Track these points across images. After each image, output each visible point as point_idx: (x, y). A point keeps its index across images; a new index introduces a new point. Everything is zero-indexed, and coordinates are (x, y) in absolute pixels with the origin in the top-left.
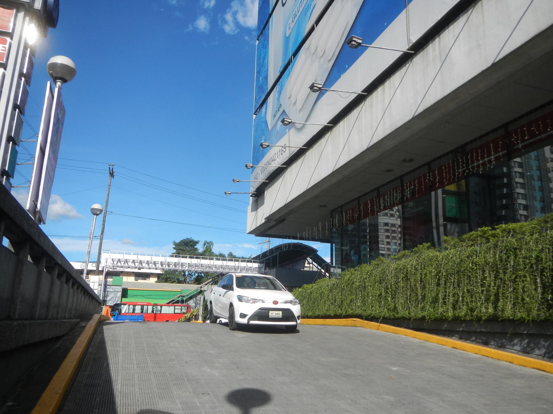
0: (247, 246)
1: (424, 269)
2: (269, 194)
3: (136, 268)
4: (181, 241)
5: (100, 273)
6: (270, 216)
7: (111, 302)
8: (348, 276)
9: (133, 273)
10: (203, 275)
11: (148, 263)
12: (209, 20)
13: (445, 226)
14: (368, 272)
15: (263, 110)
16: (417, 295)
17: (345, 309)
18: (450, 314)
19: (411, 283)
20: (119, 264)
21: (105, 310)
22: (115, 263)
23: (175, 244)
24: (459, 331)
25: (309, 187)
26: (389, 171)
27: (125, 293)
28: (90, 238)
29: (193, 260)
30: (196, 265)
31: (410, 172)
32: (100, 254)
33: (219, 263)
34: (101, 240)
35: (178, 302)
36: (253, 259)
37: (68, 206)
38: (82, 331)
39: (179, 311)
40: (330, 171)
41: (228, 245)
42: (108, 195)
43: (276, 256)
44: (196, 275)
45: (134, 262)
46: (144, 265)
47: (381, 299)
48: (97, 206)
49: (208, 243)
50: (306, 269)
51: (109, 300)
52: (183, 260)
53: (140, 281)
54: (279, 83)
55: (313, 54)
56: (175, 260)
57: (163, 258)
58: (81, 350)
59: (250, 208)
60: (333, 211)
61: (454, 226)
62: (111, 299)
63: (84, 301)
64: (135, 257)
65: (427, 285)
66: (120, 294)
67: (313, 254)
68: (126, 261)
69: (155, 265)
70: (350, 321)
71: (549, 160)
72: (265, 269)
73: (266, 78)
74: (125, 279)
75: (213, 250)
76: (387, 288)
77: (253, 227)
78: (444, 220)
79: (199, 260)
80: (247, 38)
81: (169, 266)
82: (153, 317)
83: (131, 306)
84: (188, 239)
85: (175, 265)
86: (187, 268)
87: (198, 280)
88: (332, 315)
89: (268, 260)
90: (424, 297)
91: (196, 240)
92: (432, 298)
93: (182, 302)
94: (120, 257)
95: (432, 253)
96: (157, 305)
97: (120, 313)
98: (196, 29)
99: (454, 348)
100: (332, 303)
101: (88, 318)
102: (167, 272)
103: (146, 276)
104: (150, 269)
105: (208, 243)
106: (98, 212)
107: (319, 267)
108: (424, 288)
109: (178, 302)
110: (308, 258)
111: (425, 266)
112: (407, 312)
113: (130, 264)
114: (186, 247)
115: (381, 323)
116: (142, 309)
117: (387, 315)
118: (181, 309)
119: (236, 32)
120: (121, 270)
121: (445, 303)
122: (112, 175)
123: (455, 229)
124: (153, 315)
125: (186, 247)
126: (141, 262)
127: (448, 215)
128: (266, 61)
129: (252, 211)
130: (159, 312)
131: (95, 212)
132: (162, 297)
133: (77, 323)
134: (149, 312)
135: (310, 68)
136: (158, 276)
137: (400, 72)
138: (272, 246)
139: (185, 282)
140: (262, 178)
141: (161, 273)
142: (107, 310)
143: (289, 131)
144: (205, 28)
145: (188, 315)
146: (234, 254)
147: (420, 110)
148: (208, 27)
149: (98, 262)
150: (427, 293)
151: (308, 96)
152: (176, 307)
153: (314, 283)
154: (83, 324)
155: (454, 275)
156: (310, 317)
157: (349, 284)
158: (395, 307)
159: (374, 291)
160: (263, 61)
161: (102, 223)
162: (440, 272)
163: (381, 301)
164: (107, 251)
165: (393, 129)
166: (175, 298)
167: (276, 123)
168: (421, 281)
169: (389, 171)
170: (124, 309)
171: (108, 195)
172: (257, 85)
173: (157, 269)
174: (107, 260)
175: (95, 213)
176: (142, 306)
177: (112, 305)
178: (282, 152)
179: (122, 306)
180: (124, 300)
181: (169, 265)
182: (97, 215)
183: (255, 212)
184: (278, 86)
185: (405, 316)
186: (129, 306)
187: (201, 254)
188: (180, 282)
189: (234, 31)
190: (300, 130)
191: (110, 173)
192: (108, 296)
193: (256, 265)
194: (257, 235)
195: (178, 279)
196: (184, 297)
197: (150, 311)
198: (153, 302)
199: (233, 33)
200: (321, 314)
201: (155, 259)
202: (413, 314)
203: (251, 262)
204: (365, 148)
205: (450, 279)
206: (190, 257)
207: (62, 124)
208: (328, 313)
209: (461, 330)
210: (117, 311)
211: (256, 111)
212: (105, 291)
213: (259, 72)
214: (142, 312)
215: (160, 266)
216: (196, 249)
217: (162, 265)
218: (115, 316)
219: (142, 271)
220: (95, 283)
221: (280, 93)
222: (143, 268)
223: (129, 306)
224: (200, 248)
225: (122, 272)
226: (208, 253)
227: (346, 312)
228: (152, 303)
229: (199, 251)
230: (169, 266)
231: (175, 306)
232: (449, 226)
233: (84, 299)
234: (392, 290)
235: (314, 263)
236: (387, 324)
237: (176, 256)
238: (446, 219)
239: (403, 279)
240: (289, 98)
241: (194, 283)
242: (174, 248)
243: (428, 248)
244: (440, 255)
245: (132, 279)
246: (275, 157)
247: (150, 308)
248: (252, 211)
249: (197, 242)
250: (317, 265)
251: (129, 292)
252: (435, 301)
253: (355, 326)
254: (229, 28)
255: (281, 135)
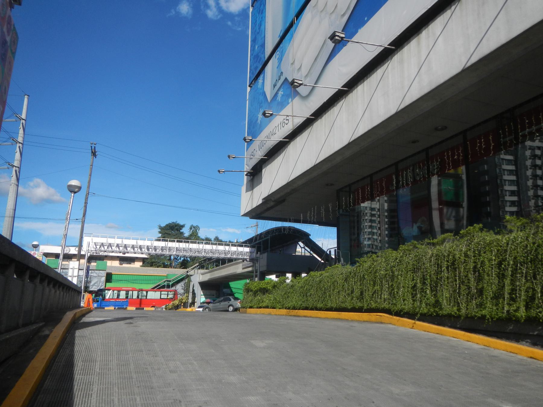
0: (230, 230)
1: (480, 255)
2: (267, 172)
3: (120, 252)
4: (167, 225)
5: (80, 257)
6: (268, 196)
7: (94, 287)
8: (369, 263)
9: (118, 257)
10: (189, 259)
11: (133, 247)
12: (191, 5)
13: (441, 211)
14: (397, 259)
15: (260, 80)
16: (469, 288)
17: (367, 301)
18: (522, 313)
19: (460, 273)
20: (102, 249)
21: (85, 300)
22: (98, 247)
23: (161, 228)
24: (534, 335)
25: (318, 162)
26: (414, 142)
27: (109, 278)
28: (67, 219)
29: (181, 244)
30: (184, 250)
31: (440, 143)
32: (81, 238)
33: (208, 247)
34: (83, 223)
35: (163, 287)
36: (243, 243)
37: (52, 190)
38: (42, 345)
39: (165, 297)
40: (345, 142)
41: (212, 230)
42: (90, 175)
43: (268, 240)
44: (182, 259)
45: (118, 246)
46: (129, 249)
47: (416, 290)
48: (74, 183)
49: (194, 228)
50: (297, 254)
51: (93, 285)
52: (170, 244)
53: (125, 265)
54: (279, 49)
55: (322, 11)
56: (162, 244)
57: (150, 242)
58: (27, 393)
59: (244, 188)
60: (339, 191)
61: (450, 210)
62: (95, 283)
63: (55, 295)
64: (119, 241)
65: (486, 277)
66: (104, 279)
67: (305, 238)
68: (110, 245)
69: (141, 250)
70: (373, 316)
71: (528, 147)
72: (257, 253)
73: (263, 46)
74: (109, 263)
75: (199, 235)
76: (424, 279)
77: (249, 209)
78: (440, 204)
79: (187, 244)
80: (229, 23)
81: (155, 250)
82: (139, 303)
83: (115, 292)
84: (173, 223)
85: (162, 249)
86: (174, 253)
87: (184, 264)
88: (349, 308)
89: (258, 243)
90: (481, 292)
91: (182, 224)
92: (493, 292)
93: (168, 286)
94: (104, 240)
95: (489, 237)
96: (142, 290)
97: (104, 298)
98: (178, 13)
99: (531, 358)
100: (348, 294)
101: (63, 311)
102: (152, 256)
103: (131, 260)
104: (135, 253)
105: (194, 228)
106: (76, 190)
107: (311, 252)
108: (479, 279)
109: (163, 287)
110: (300, 243)
111: (480, 252)
112: (455, 308)
113: (114, 248)
114: (171, 231)
115: (419, 320)
116: (127, 294)
117: (425, 311)
118: (168, 294)
119: (219, 17)
120: (106, 254)
121: (513, 300)
122: (94, 154)
123: (451, 213)
124: (139, 300)
125: (171, 231)
126: (126, 247)
127: (444, 198)
128: (262, 27)
129: (247, 191)
130: (145, 298)
131: (72, 189)
132: (147, 281)
133: (39, 330)
134: (134, 298)
135: (313, 31)
136: (143, 260)
137: (442, 17)
138: (260, 230)
139: (170, 266)
140: (259, 154)
141: (146, 257)
142: (89, 299)
143: (292, 101)
144: (187, 13)
145: (176, 302)
146: (220, 238)
147: (474, 59)
148: (191, 12)
149: (80, 246)
150: (485, 285)
151: (316, 59)
152: (162, 293)
153: (324, 270)
154: (47, 332)
155: (527, 263)
156: (320, 309)
157: (371, 273)
158: (437, 302)
159: (405, 282)
160: (259, 28)
161: (84, 204)
162: (504, 260)
163: (416, 294)
164: (90, 235)
165: (434, 86)
166: (161, 283)
167: (276, 94)
168: (475, 272)
169: (414, 142)
170: (109, 295)
171: (90, 175)
172: (251, 55)
173: (142, 254)
174: (90, 245)
175: (73, 190)
176: (127, 292)
177: (96, 290)
178: (283, 124)
179: (106, 291)
180: (109, 285)
181: (155, 249)
182: (75, 193)
183: (250, 193)
184: (278, 53)
185: (453, 313)
186: (113, 291)
187: (187, 238)
188: (165, 266)
189: (217, 16)
190: (305, 98)
191: (92, 152)
192: (90, 282)
193: (247, 250)
194: (252, 218)
195: (164, 264)
196: (170, 281)
197: (135, 297)
198: (138, 287)
199: (215, 19)
200: (334, 305)
201: (141, 243)
202: (463, 311)
203: (241, 246)
204: (393, 111)
205: (520, 269)
206: (178, 241)
207: (14, 53)
208: (343, 305)
209: (536, 333)
210: (101, 297)
211: (251, 83)
212: (87, 275)
213: (254, 41)
214: (127, 297)
215: (146, 251)
216: (182, 233)
217: (148, 249)
218: (98, 301)
219: (127, 255)
220: (73, 272)
221: (280, 60)
222: (128, 253)
223: (113, 291)
224: (186, 232)
225: (106, 256)
226: (194, 237)
227: (368, 306)
228: (137, 288)
229: (185, 235)
230: (155, 250)
231: (161, 292)
232: (445, 210)
233: (56, 292)
234: (431, 281)
235: (306, 248)
236: (424, 321)
237: (163, 240)
238: (441, 202)
239: (447, 268)
240: (292, 64)
241: (180, 267)
242: (160, 232)
243: (481, 230)
244: (503, 239)
245: (116, 263)
246: (276, 129)
247: (135, 293)
248: (247, 191)
249: (183, 226)
250: (309, 250)
251: (113, 277)
252: (497, 296)
253: (382, 323)
254: (211, 13)
255: (282, 105)
